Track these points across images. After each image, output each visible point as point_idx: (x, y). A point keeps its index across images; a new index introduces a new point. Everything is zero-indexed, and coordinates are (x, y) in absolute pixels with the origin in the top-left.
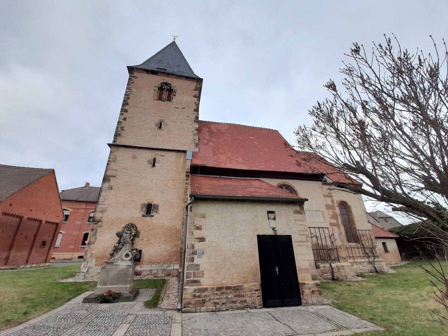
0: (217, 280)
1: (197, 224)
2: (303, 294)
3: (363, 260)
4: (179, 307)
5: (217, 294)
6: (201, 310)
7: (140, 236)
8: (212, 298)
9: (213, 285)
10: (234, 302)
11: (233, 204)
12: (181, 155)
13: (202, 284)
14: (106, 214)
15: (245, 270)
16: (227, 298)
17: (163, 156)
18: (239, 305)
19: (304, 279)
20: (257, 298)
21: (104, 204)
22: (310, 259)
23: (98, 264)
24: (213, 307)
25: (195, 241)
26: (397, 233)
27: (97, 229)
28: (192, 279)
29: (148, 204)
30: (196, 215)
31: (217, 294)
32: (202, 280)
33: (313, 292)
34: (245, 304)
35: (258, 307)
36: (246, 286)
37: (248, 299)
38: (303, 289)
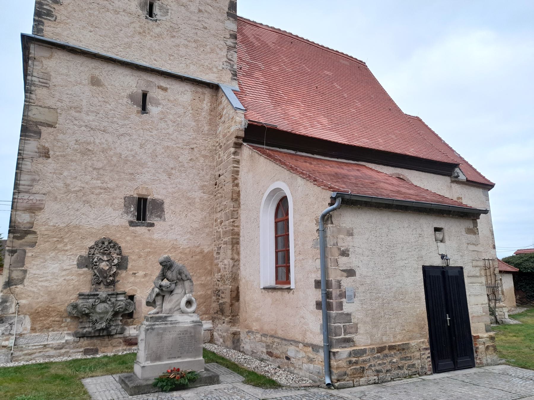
0: (376, 336)
1: (343, 245)
2: (476, 352)
4: (328, 381)
5: (378, 358)
6: (361, 383)
7: (129, 266)
8: (373, 363)
9: (371, 345)
10: (399, 368)
11: (390, 213)
12: (204, 94)
13: (357, 343)
14: (41, 217)
15: (410, 321)
16: (386, 363)
17: (165, 89)
18: (406, 372)
19: (477, 331)
20: (424, 359)
21: (34, 190)
22: (484, 302)
23: (38, 326)
24: (376, 377)
25: (342, 276)
26: (516, 265)
27: (25, 252)
28: (342, 336)
29: (140, 199)
30: (340, 231)
31: (378, 358)
32: (356, 338)
34: (414, 370)
35: (429, 373)
36: (413, 343)
37: (417, 362)
38: (476, 344)
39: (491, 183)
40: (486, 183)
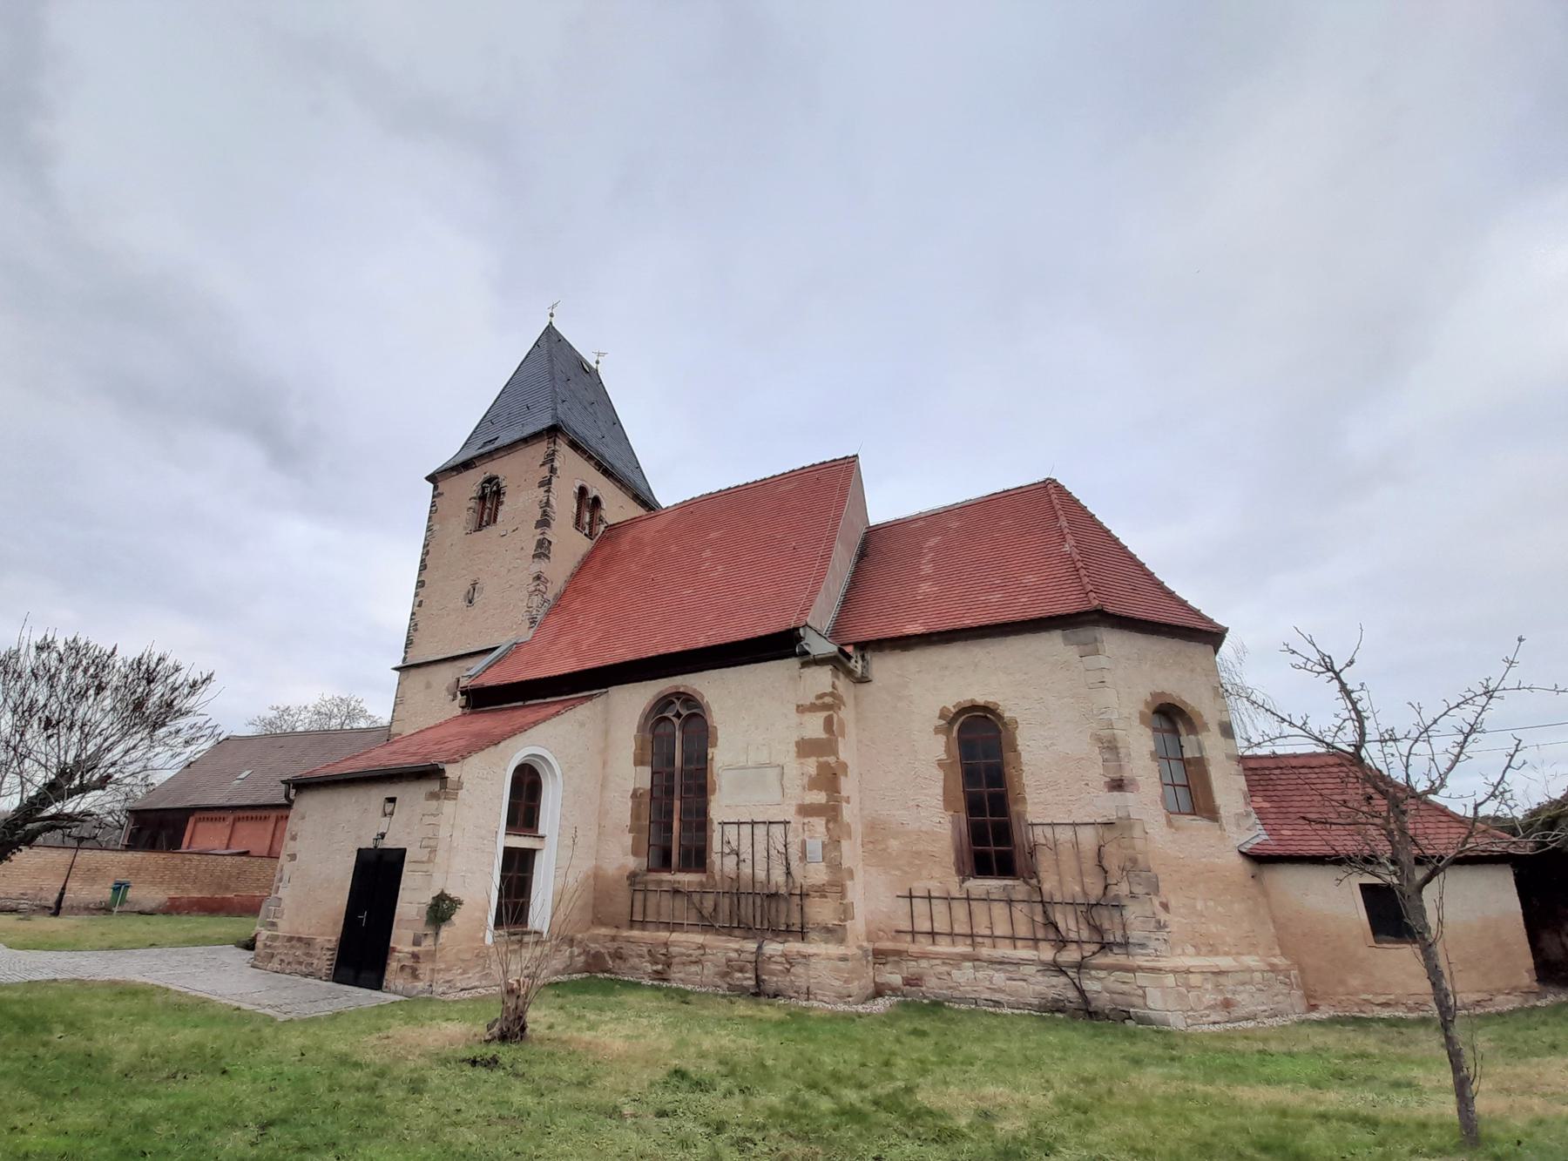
3: (1024, 953)
10: (300, 963)
20: (324, 961)
33: (403, 968)
36: (320, 939)
39: (1218, 626)
40: (1203, 626)
